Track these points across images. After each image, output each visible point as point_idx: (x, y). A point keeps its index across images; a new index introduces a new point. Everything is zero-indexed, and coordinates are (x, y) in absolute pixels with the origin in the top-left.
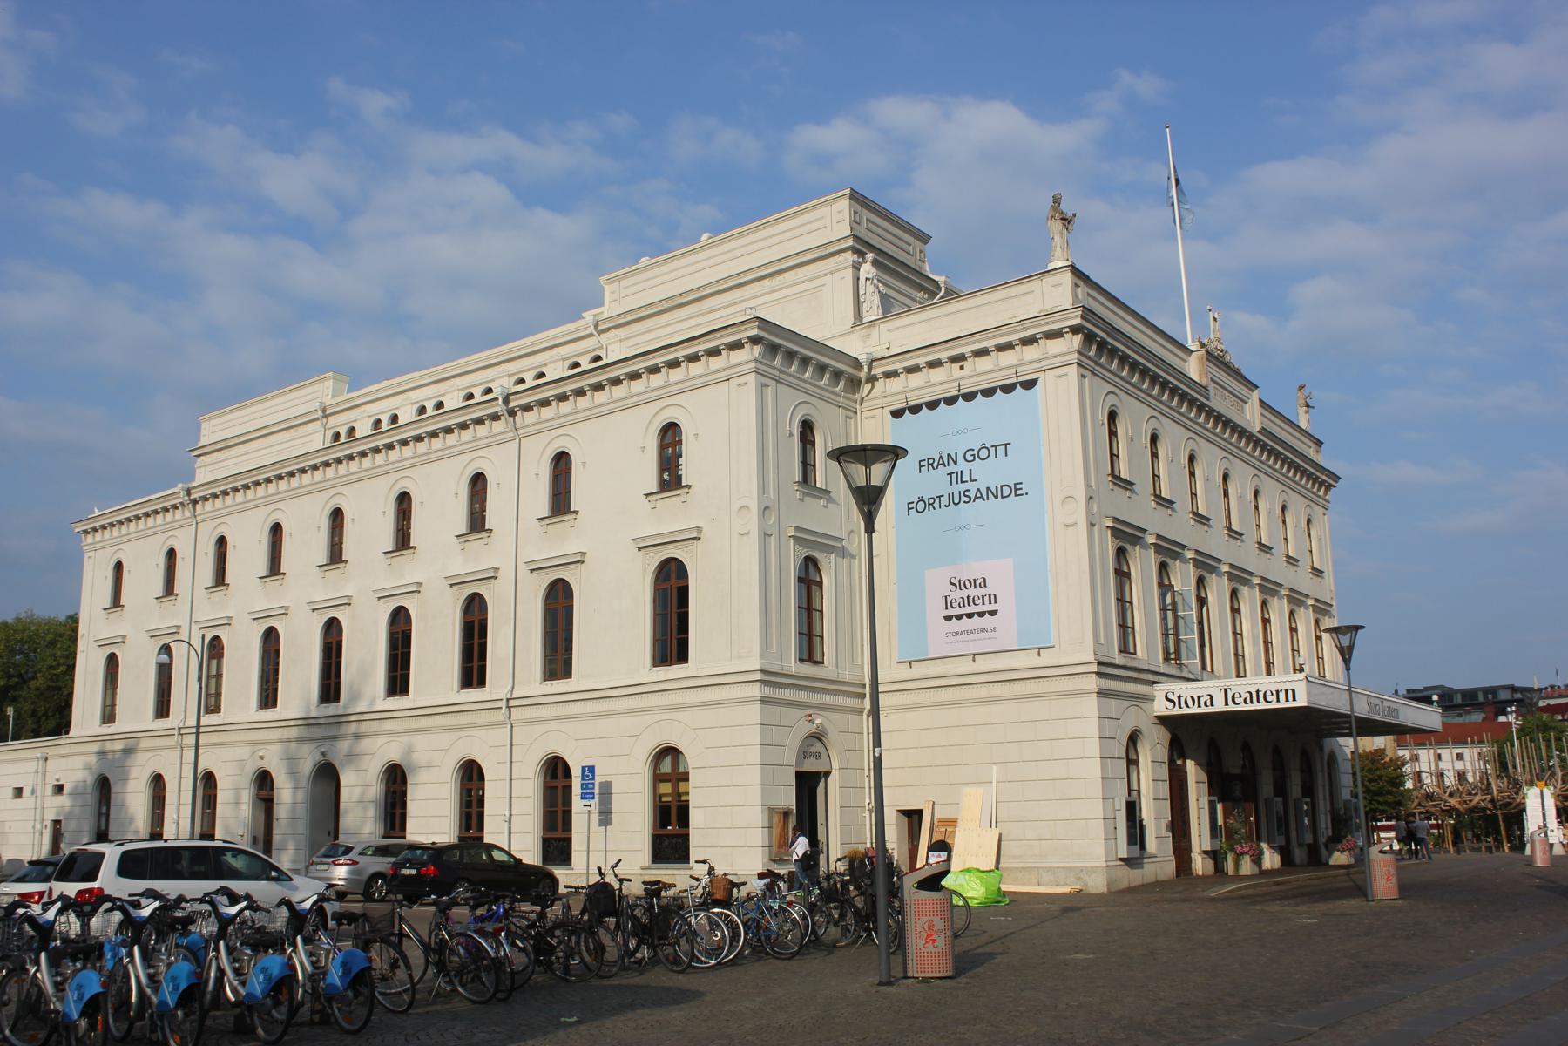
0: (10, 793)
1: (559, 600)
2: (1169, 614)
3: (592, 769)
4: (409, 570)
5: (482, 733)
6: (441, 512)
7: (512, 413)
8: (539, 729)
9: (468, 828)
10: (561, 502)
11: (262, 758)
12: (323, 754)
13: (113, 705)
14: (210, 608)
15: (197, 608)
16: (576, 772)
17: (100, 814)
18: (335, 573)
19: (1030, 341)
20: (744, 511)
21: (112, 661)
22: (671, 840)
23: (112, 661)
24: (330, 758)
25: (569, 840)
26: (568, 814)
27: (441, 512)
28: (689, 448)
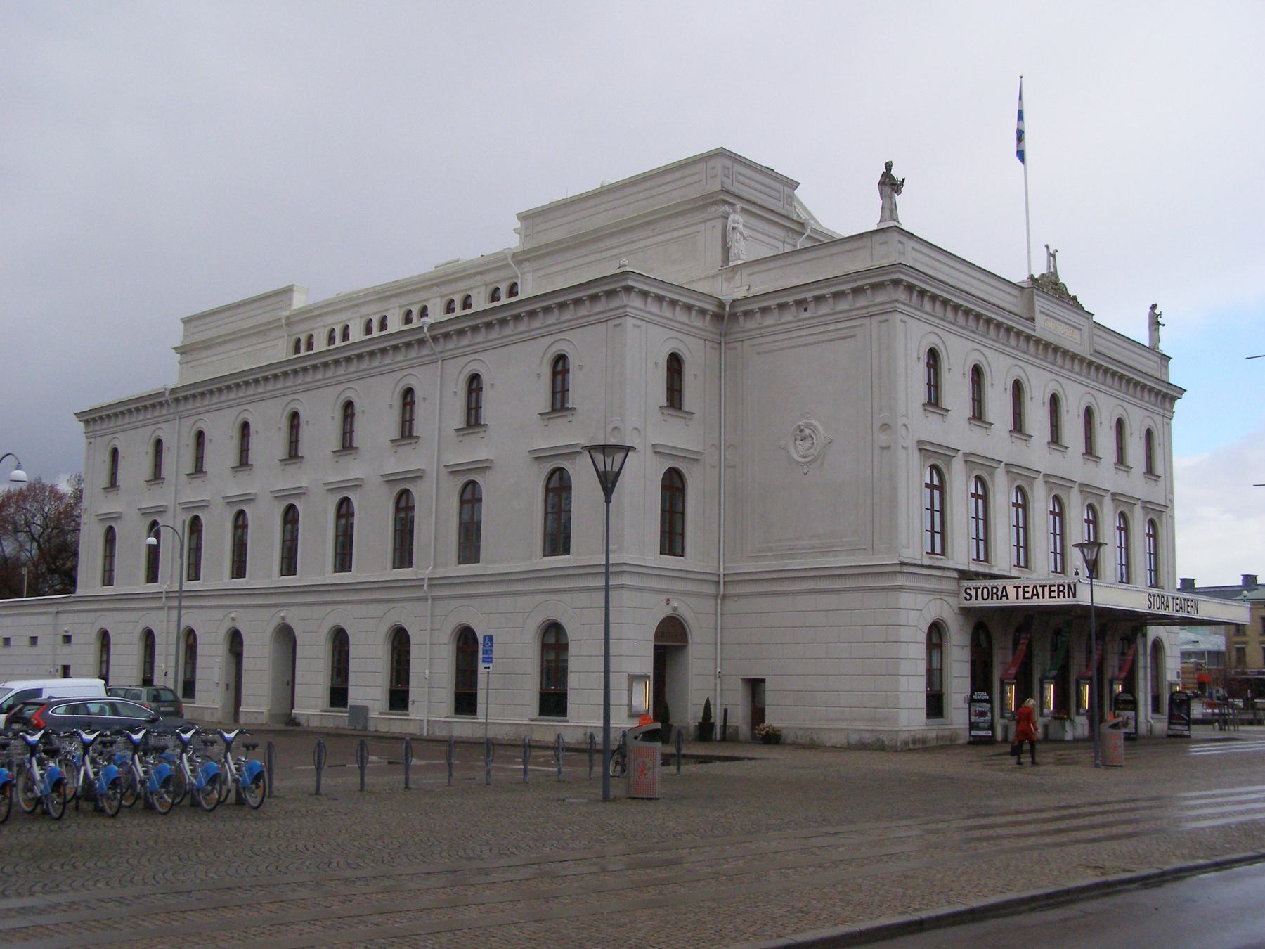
0: (27, 641)
1: (470, 497)
2: (981, 522)
3: (491, 638)
4: (354, 469)
5: (566, 597)
6: (378, 421)
7: (435, 338)
8: (453, 604)
9: (398, 682)
10: (473, 419)
11: (233, 619)
12: (283, 618)
13: (111, 570)
14: (193, 493)
15: (178, 492)
16: (480, 640)
17: (101, 662)
18: (243, 475)
19: (857, 291)
20: (616, 432)
21: (110, 532)
22: (553, 701)
23: (110, 532)
24: (288, 621)
25: (407, 692)
26: (474, 672)
27: (378, 421)
28: (487, 395)
